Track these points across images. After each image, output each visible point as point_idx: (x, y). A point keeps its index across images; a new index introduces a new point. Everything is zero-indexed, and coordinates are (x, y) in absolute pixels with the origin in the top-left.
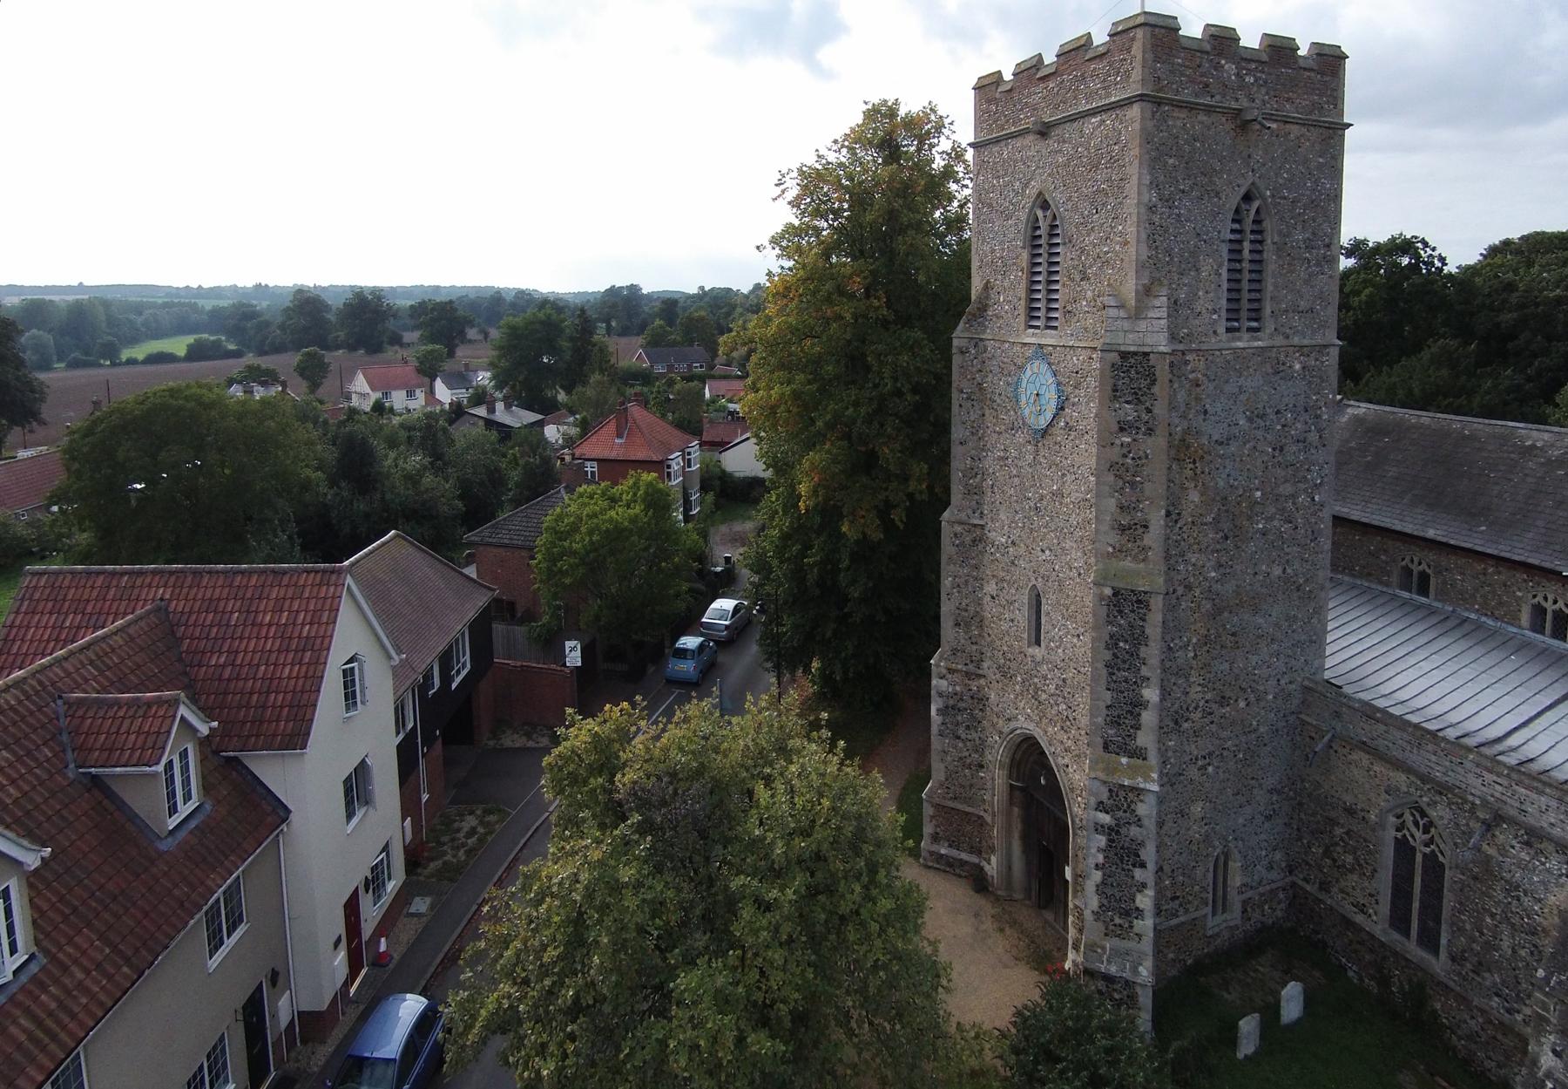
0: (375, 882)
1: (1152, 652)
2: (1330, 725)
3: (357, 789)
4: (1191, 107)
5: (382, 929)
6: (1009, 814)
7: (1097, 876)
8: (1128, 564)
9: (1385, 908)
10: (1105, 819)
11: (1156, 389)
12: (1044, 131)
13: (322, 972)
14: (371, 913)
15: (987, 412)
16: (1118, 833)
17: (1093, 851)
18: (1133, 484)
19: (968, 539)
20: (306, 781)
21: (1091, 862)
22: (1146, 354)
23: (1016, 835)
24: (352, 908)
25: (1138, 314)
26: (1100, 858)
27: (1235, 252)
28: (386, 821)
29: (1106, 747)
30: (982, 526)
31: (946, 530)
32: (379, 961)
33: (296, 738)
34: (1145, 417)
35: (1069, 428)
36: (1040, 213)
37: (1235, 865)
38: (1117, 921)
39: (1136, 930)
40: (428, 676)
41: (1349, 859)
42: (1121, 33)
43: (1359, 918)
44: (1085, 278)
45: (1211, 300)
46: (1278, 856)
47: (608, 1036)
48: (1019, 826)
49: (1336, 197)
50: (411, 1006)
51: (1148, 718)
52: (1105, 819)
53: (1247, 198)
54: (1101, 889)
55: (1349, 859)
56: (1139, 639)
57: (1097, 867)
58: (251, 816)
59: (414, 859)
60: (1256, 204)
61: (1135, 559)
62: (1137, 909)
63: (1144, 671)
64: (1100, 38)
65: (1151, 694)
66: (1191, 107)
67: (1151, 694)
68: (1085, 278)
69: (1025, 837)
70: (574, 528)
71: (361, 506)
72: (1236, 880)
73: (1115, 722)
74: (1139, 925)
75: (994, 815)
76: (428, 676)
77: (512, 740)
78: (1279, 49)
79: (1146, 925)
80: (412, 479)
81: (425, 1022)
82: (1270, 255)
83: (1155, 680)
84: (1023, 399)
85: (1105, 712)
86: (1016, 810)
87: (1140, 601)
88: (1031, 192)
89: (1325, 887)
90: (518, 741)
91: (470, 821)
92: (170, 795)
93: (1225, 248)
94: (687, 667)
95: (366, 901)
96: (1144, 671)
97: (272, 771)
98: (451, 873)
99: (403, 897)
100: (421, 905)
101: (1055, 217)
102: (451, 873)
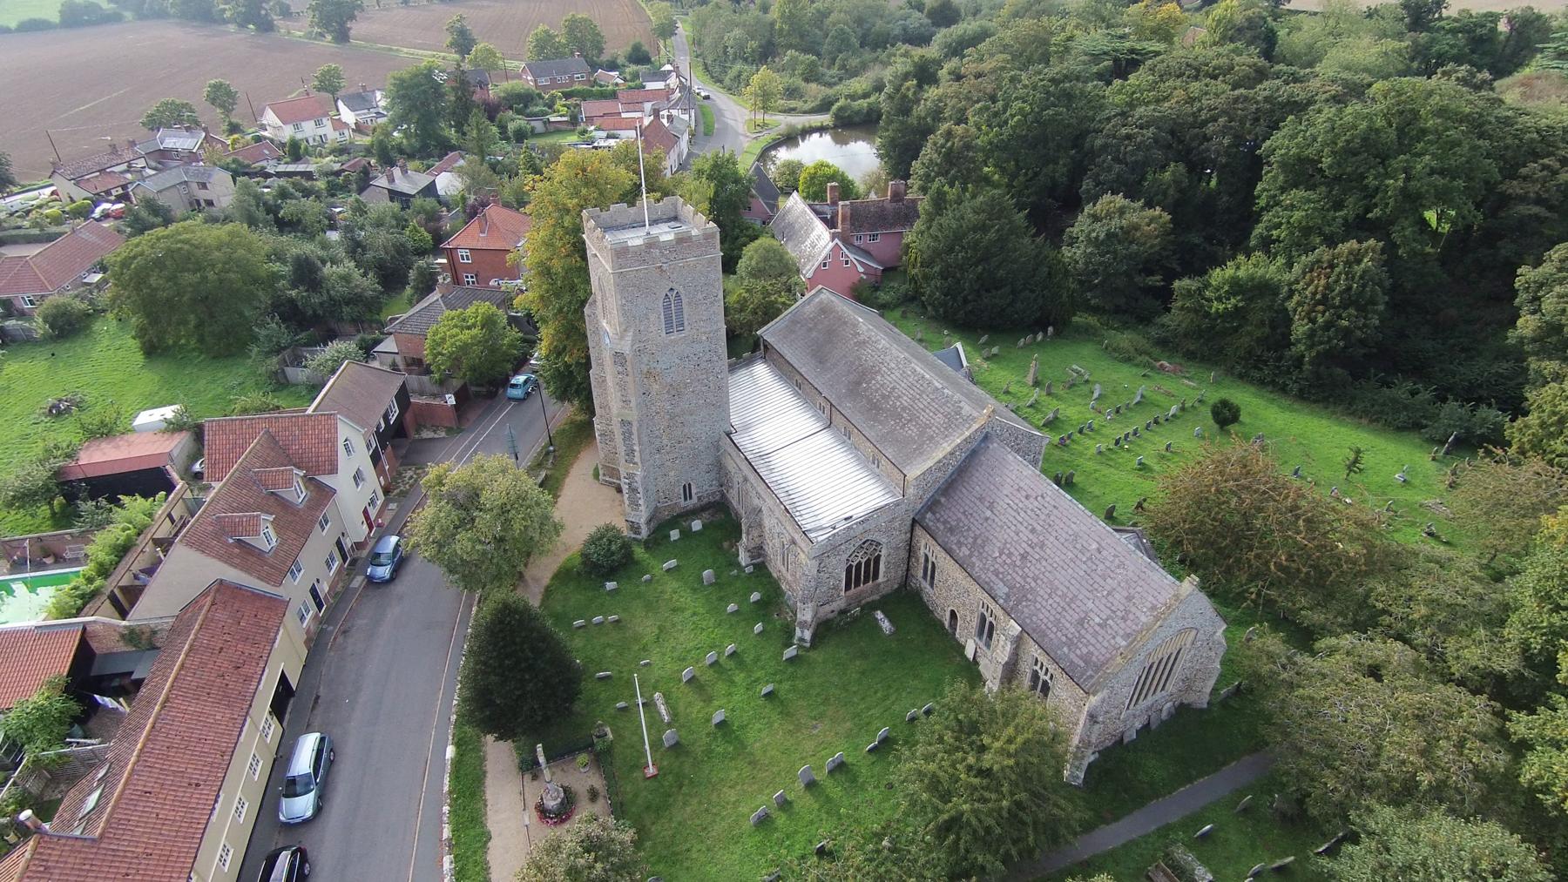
0: (372, 502)
1: (635, 437)
2: (722, 448)
3: (358, 477)
5: (379, 515)
13: (360, 532)
14: (373, 513)
20: (341, 482)
24: (365, 512)
25: (622, 338)
28: (373, 482)
32: (379, 526)
33: (333, 470)
40: (378, 427)
45: (657, 321)
47: (441, 546)
50: (394, 539)
56: (631, 433)
58: (323, 494)
59: (386, 491)
65: (636, 448)
70: (443, 339)
71: (315, 299)
76: (378, 427)
77: (426, 434)
80: (346, 278)
81: (397, 545)
82: (686, 308)
90: (430, 435)
91: (410, 473)
92: (298, 494)
94: (517, 393)
95: (370, 509)
97: (326, 479)
98: (403, 494)
99: (385, 505)
100: (393, 506)
102: (403, 494)
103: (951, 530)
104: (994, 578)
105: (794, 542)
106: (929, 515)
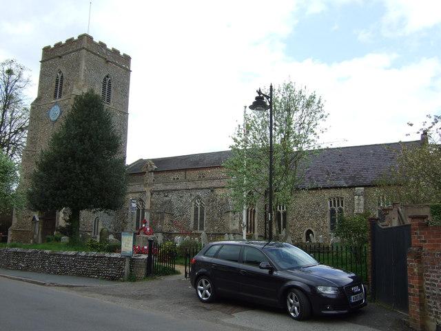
4: (95, 54)
12: (60, 57)
19: (31, 155)
27: (104, 87)
31: (10, 233)
37: (100, 223)
42: (81, 37)
44: (69, 85)
49: (129, 84)
53: (107, 77)
64: (76, 38)
66: (95, 54)
78: (116, 52)
84: (51, 115)
105: (212, 189)
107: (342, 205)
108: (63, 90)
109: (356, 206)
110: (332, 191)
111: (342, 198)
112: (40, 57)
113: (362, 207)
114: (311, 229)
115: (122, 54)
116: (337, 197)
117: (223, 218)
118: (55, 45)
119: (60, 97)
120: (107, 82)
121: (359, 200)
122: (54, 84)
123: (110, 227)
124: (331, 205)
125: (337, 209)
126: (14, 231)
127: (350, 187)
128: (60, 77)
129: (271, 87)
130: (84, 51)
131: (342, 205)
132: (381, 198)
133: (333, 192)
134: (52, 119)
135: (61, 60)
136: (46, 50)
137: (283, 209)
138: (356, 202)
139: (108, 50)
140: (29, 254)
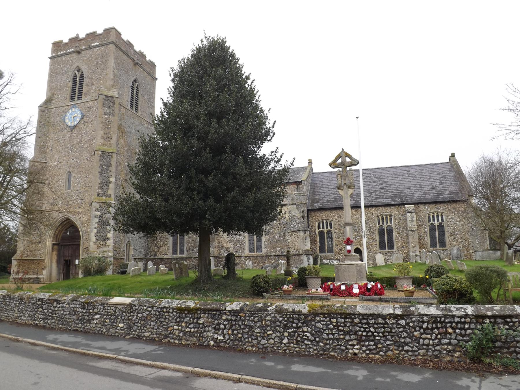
1: (113, 168)
6: (52, 254)
7: (95, 231)
8: (106, 147)
9: (171, 250)
10: (98, 213)
11: (115, 106)
15: (51, 129)
16: (102, 217)
17: (94, 223)
18: (108, 128)
21: (93, 227)
22: (112, 97)
23: (54, 261)
26: (96, 225)
29: (98, 195)
30: (46, 163)
31: (14, 263)
34: (112, 112)
35: (85, 122)
36: (77, 72)
37: (131, 248)
38: (101, 243)
39: (107, 244)
41: (162, 243)
42: (108, 31)
43: (165, 257)
44: (93, 84)
46: (143, 250)
48: (56, 258)
49: (154, 94)
51: (111, 186)
52: (98, 213)
53: (135, 81)
54: (96, 235)
55: (162, 243)
56: (109, 165)
57: (95, 228)
60: (137, 84)
61: (108, 146)
62: (108, 238)
63: (111, 173)
65: (112, 179)
67: (112, 179)
68: (93, 84)
69: (58, 262)
72: (132, 252)
73: (101, 188)
74: (108, 243)
75: (46, 255)
79: (110, 243)
82: (140, 96)
83: (114, 176)
85: (98, 185)
86: (55, 253)
87: (110, 155)
88: (75, 65)
89: (155, 255)
93: (131, 89)
96: (111, 173)
101: (82, 72)
103: (334, 201)
104: (379, 200)
106: (315, 204)
107: (391, 223)
108: (85, 90)
109: (409, 224)
110: (381, 209)
111: (391, 216)
112: (49, 53)
113: (415, 223)
114: (359, 247)
115: (147, 59)
116: (386, 215)
117: (287, 238)
118: (71, 40)
119: (80, 98)
120: (135, 86)
121: (412, 217)
122: (70, 84)
123: (141, 252)
124: (319, 228)
125: (385, 226)
126: (214, 257)
127: (398, 205)
128: (78, 75)
129: (275, 122)
130: (112, 46)
131: (331, 227)
132: (431, 214)
133: (382, 210)
134: (69, 124)
135: (80, 56)
136: (57, 45)
137: (438, 220)
138: (409, 219)
139: (135, 51)
140: (233, 312)
